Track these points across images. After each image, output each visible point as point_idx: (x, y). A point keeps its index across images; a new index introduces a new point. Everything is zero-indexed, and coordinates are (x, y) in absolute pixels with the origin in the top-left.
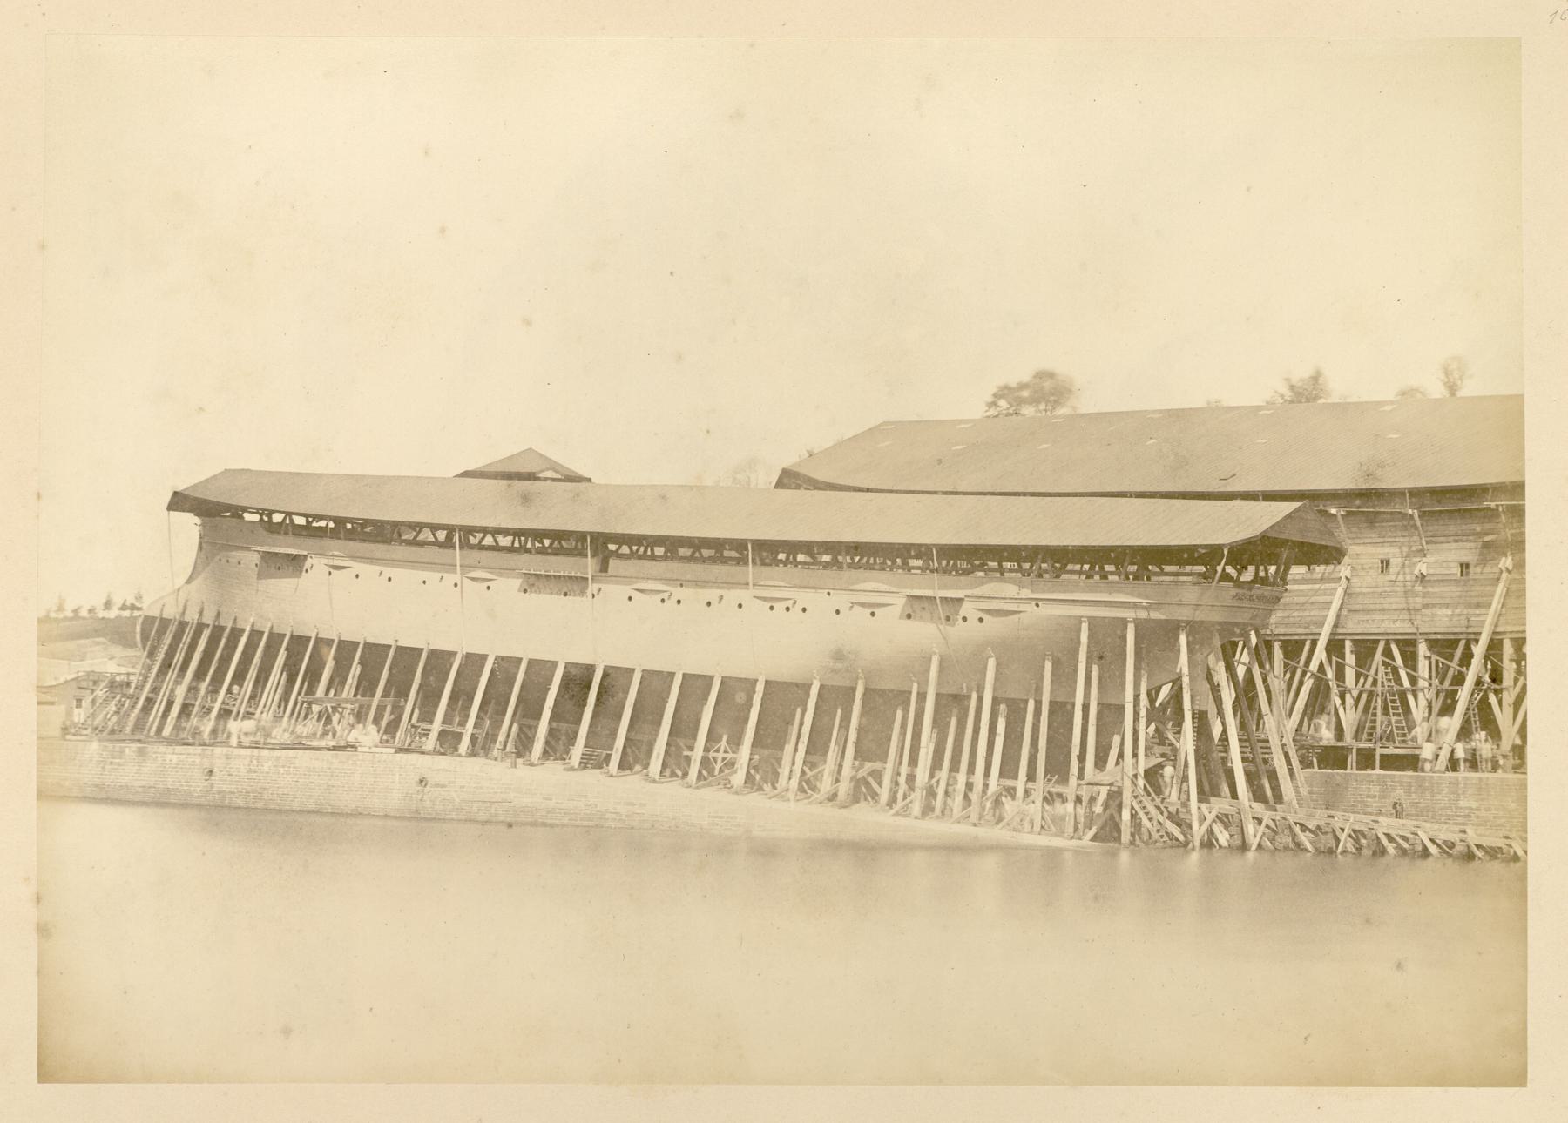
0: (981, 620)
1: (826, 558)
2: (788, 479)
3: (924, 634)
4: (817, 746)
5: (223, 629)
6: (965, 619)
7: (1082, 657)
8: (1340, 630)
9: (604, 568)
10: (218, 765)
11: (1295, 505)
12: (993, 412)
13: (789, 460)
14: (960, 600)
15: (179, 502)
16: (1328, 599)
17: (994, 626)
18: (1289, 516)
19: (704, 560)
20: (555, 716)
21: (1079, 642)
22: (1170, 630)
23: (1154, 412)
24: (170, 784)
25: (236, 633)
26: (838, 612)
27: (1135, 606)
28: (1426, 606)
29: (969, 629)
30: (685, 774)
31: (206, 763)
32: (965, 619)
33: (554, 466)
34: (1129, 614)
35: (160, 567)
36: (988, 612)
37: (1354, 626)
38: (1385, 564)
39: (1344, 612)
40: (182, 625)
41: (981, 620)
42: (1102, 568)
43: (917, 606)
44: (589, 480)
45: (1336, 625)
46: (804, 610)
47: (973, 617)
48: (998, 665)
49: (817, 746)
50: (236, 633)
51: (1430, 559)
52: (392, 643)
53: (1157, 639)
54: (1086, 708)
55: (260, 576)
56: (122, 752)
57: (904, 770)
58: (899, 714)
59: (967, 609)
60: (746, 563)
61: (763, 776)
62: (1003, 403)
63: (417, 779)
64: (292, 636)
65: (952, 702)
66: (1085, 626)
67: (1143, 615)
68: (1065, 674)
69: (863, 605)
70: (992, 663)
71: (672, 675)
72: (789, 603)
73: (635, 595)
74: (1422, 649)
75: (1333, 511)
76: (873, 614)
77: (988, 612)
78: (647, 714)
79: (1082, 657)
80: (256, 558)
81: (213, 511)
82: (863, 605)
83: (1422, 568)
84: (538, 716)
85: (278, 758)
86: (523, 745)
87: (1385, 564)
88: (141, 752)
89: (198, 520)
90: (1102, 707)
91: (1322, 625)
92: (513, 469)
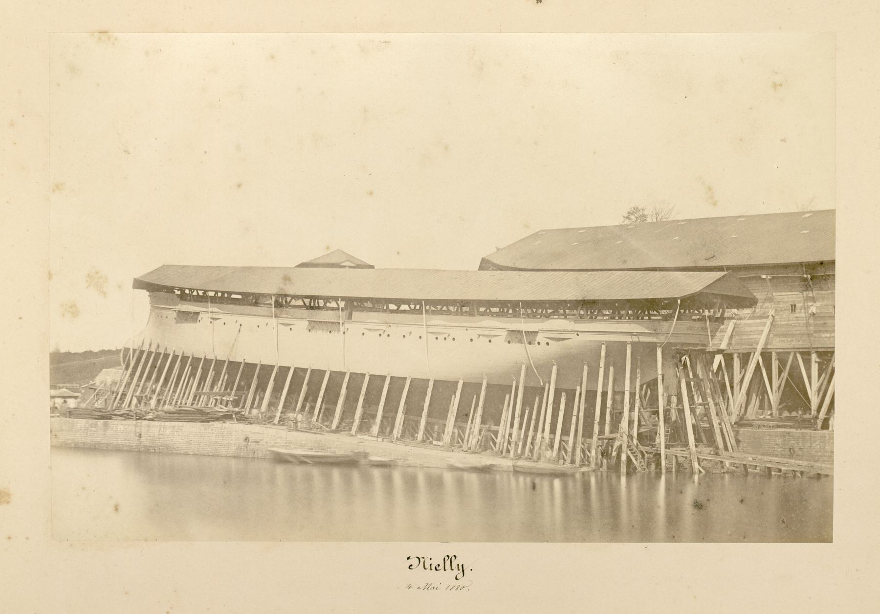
0: (548, 344)
1: (482, 309)
2: (485, 265)
3: (517, 353)
4: (463, 416)
5: (160, 354)
6: (539, 343)
7: (602, 364)
8: (769, 347)
9: (350, 316)
10: (144, 431)
11: (722, 274)
12: (627, 222)
13: (487, 251)
14: (536, 333)
15: (140, 284)
16: (760, 328)
17: (555, 347)
18: (719, 280)
19: (493, 314)
20: (429, 414)
21: (600, 355)
22: (651, 348)
23: (682, 221)
24: (120, 442)
25: (166, 356)
26: (471, 340)
27: (631, 334)
28: (816, 332)
29: (540, 351)
30: (350, 429)
31: (138, 430)
32: (539, 343)
33: (350, 258)
34: (628, 339)
35: (127, 323)
36: (552, 339)
37: (778, 344)
38: (793, 308)
39: (771, 335)
40: (158, 355)
41: (548, 344)
42: (619, 313)
43: (515, 335)
44: (372, 267)
45: (766, 344)
46: (454, 339)
47: (543, 343)
48: (558, 370)
49: (463, 416)
50: (166, 356)
51: (818, 304)
52: (213, 358)
53: (645, 353)
54: (632, 395)
55: (177, 323)
56: (96, 424)
57: (531, 433)
58: (507, 396)
59: (540, 338)
60: (422, 313)
61: (432, 434)
62: (633, 217)
63: (244, 438)
64: (193, 358)
65: (533, 393)
66: (604, 347)
67: (635, 339)
68: (593, 375)
69: (483, 335)
70: (555, 369)
71: (289, 368)
72: (446, 336)
73: (366, 332)
74: (814, 357)
75: (764, 277)
76: (490, 341)
77: (552, 339)
78: (371, 400)
79: (602, 364)
80: (175, 315)
81: (161, 290)
82: (483, 335)
83: (813, 309)
84: (336, 403)
85: (174, 427)
86: (410, 429)
87: (793, 308)
88: (105, 425)
89: (148, 293)
90: (615, 393)
91: (757, 344)
92: (328, 261)
